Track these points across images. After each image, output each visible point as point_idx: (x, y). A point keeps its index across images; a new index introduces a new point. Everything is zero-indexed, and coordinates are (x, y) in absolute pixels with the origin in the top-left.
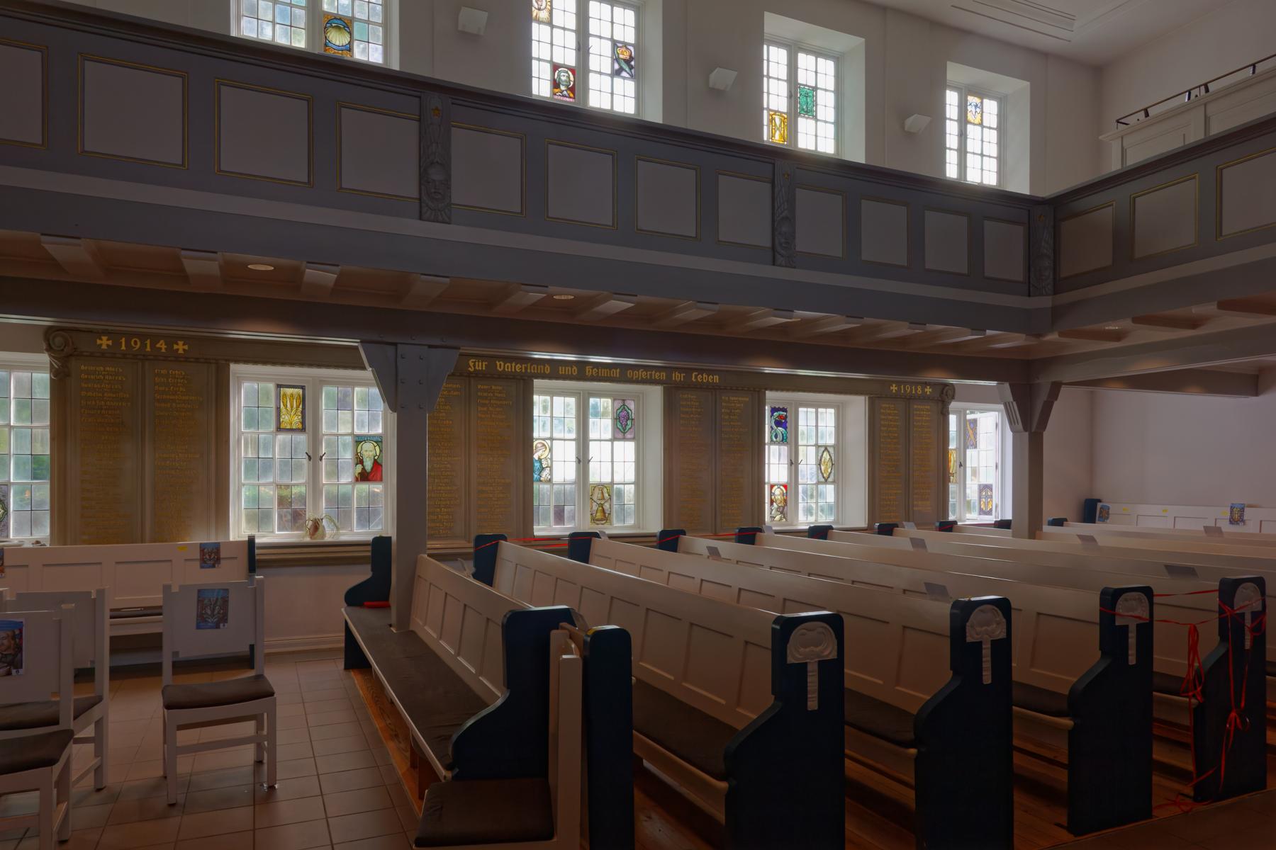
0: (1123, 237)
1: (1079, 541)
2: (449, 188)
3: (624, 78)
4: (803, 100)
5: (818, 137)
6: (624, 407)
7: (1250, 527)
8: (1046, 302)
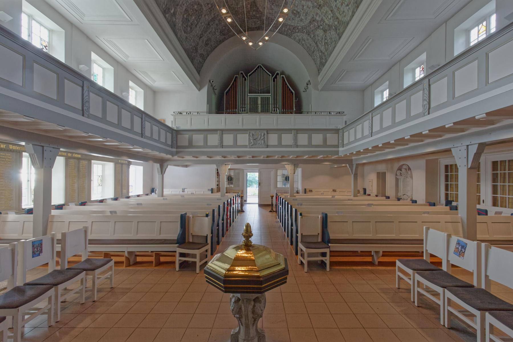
0: (190, 141)
7: (186, 193)
8: (174, 150)
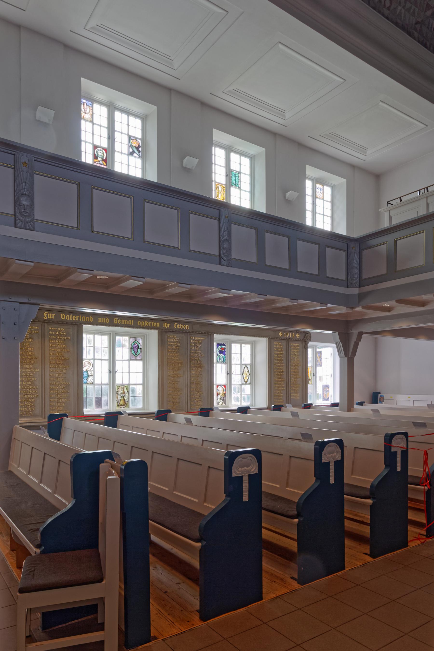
0: (392, 259)
1: (372, 413)
2: (33, 210)
3: (135, 157)
4: (233, 178)
5: (241, 198)
6: (136, 342)
8: (356, 291)
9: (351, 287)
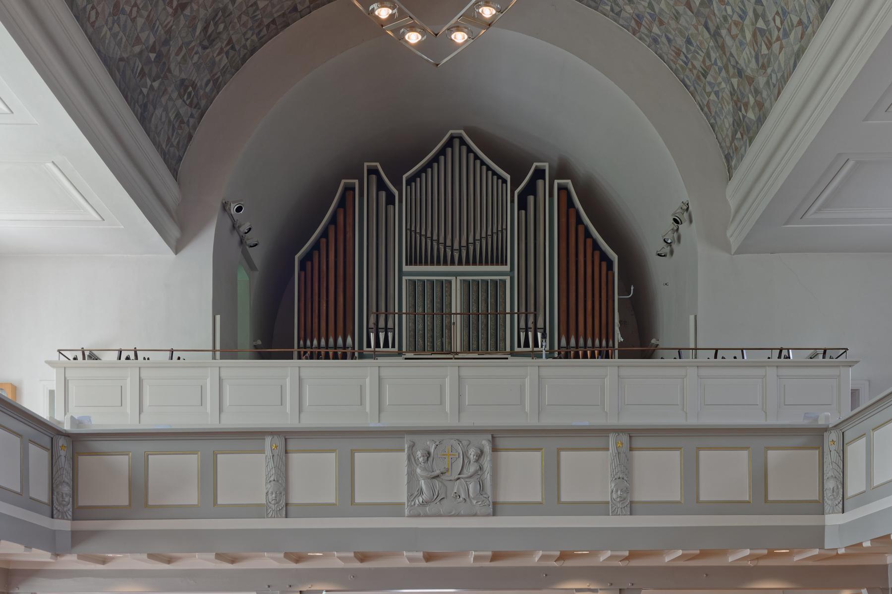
0: (138, 486)
8: (64, 525)
9: (58, 518)
